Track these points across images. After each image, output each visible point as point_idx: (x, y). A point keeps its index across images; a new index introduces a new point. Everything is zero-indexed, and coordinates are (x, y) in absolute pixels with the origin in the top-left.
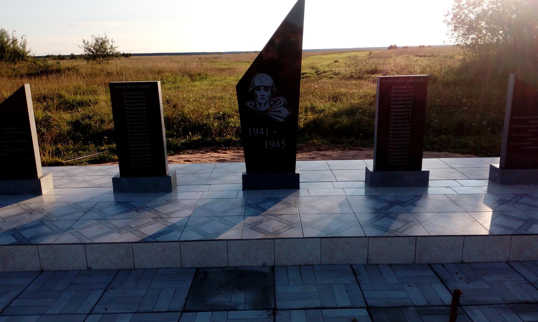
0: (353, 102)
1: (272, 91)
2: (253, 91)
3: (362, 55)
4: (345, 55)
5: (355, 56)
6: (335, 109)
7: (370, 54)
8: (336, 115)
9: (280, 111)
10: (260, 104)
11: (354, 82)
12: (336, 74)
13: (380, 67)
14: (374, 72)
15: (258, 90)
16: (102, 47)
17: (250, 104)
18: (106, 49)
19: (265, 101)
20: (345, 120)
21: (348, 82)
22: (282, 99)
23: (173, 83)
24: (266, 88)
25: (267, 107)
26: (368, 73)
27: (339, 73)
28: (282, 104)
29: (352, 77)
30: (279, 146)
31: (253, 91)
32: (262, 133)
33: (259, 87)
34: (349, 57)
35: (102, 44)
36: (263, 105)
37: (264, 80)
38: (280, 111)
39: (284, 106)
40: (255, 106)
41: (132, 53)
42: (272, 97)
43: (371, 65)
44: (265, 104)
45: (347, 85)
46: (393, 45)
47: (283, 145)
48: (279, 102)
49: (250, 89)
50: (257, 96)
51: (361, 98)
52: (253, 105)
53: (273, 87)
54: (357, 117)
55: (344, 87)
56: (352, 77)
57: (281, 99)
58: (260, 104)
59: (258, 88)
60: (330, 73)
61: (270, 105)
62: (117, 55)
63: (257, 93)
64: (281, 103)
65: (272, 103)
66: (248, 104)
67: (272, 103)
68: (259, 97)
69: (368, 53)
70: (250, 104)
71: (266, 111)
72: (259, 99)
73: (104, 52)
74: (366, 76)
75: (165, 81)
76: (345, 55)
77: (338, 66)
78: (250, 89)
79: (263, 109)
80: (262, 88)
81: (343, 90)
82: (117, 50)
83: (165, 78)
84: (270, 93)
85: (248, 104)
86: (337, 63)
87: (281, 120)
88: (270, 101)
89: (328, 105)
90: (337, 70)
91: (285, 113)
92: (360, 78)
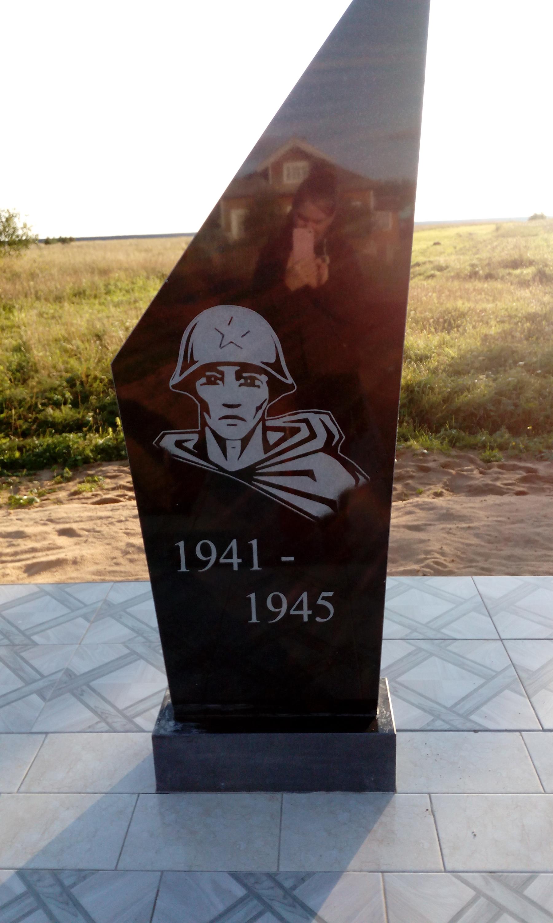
0: (484, 330)
1: (275, 387)
2: (188, 384)
3: (484, 232)
4: (452, 232)
5: (470, 234)
6: (452, 352)
7: (497, 229)
8: (457, 369)
9: (309, 473)
10: (221, 441)
11: (479, 285)
12: (441, 269)
13: (530, 255)
14: (516, 264)
15: (211, 382)
16: (9, 225)
17: (179, 444)
18: (15, 229)
19: (242, 430)
20: (482, 385)
21: (469, 285)
22: (322, 421)
23: (128, 291)
24: (244, 371)
25: (255, 453)
26: (506, 266)
27: (447, 267)
28: (319, 442)
29: (473, 275)
30: (306, 613)
31: (188, 384)
32: (235, 561)
33: (211, 366)
34: (459, 235)
35: (7, 220)
36: (234, 447)
37: (227, 335)
38: (309, 473)
39: (329, 448)
40: (201, 449)
41: (75, 236)
42: (273, 412)
43: (506, 250)
44: (245, 441)
45: (467, 291)
46: (539, 213)
47: (324, 611)
48: (305, 433)
49: (176, 379)
50: (205, 407)
51: (503, 322)
52: (190, 445)
53: (276, 366)
54: (512, 376)
55: (461, 297)
56: (473, 275)
57: (314, 419)
58: (221, 441)
59: (212, 372)
60: (428, 266)
61: (267, 447)
62: (25, 243)
63: (205, 391)
64: (313, 435)
65: (273, 437)
66: (168, 442)
67: (273, 437)
68: (216, 411)
69: (493, 227)
70: (179, 444)
71: (249, 473)
72: (214, 420)
73: (12, 235)
74: (502, 272)
75: (112, 288)
76: (452, 232)
77: (441, 253)
78: (176, 379)
79: (234, 462)
80: (230, 372)
81: (462, 305)
82: (32, 234)
83: (112, 282)
84: (262, 393)
85: (168, 442)
86: (438, 247)
87: (317, 510)
88: (266, 429)
89: (435, 340)
90: (441, 260)
91: (333, 478)
92: (489, 277)
